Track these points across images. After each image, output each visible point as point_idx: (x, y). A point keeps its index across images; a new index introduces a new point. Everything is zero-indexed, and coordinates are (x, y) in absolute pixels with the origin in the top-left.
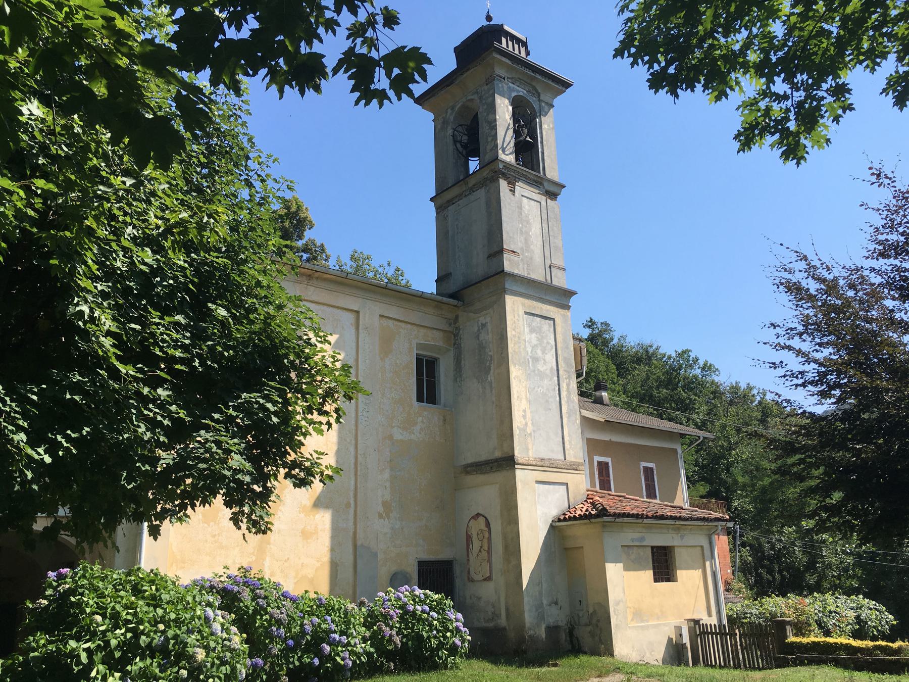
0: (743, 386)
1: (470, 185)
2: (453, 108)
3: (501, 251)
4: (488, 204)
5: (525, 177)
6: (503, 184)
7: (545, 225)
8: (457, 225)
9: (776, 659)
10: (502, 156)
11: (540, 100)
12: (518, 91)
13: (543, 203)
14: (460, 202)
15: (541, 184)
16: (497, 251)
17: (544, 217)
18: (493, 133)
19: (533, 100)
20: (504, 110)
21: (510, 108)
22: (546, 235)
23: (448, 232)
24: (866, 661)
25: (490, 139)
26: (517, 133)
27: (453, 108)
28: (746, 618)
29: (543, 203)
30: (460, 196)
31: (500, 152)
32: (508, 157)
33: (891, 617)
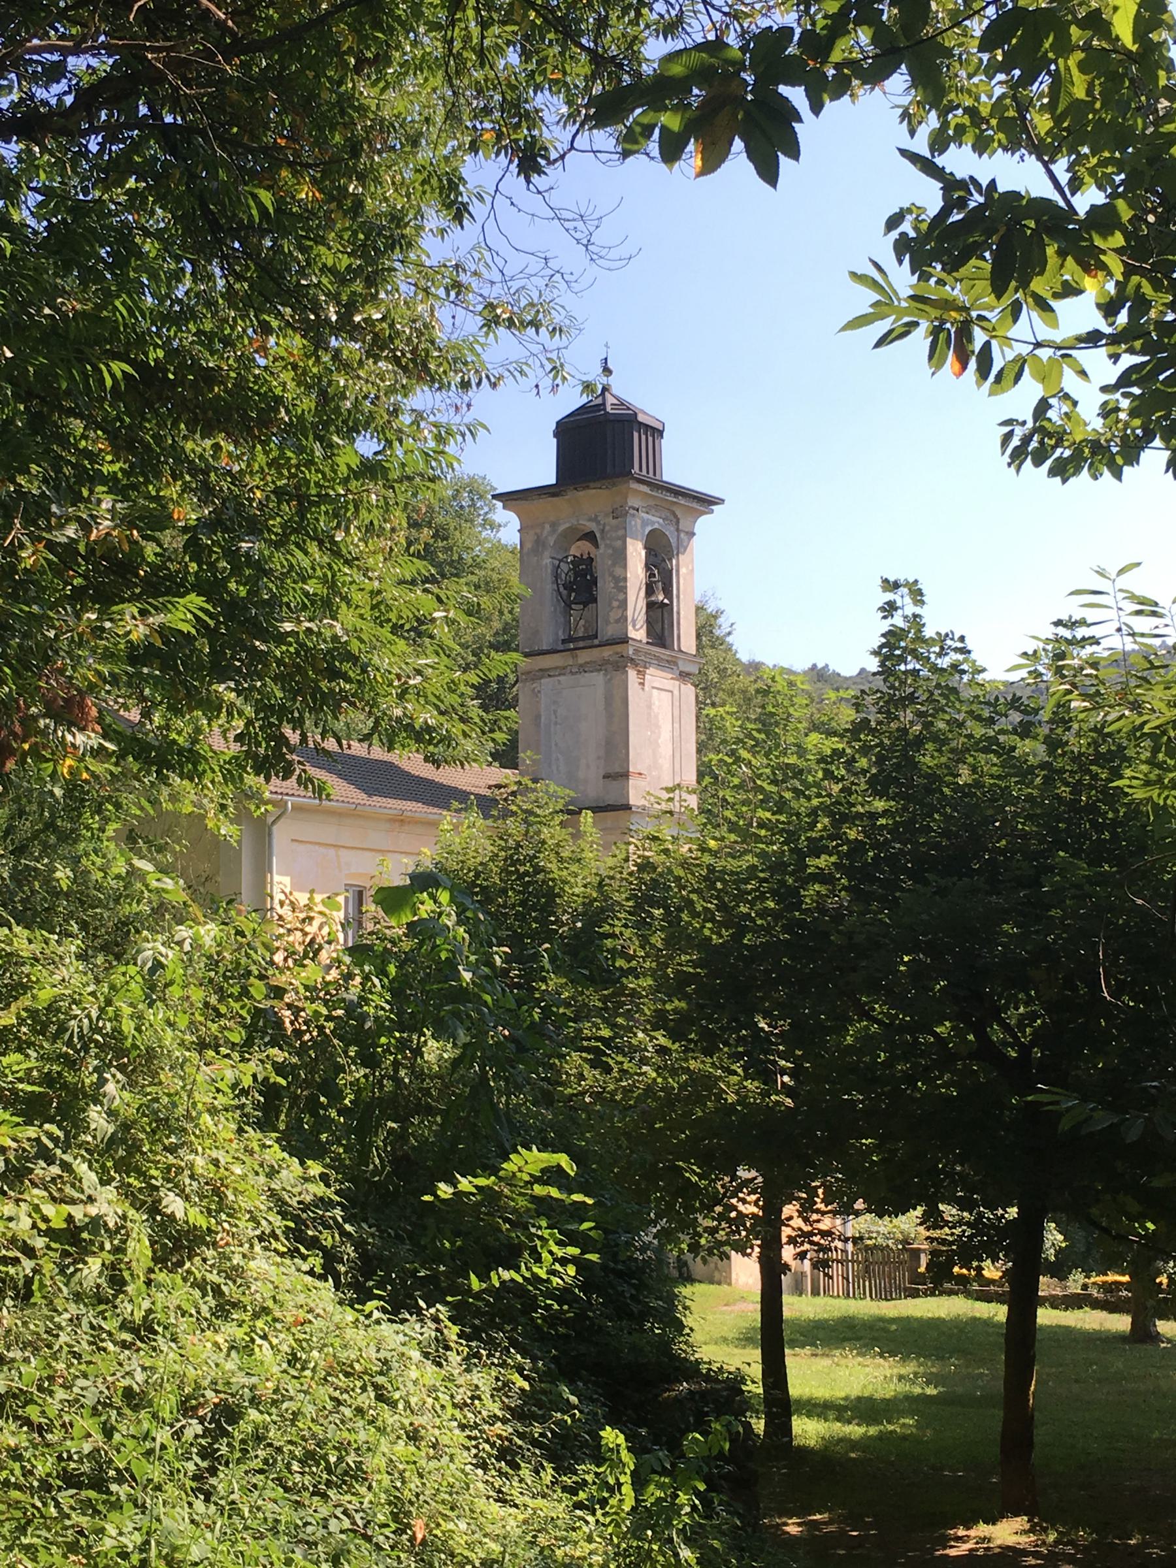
0: (820, 666)
1: (581, 661)
2: (554, 525)
3: (625, 775)
4: (608, 699)
5: (658, 658)
6: (632, 674)
7: (676, 725)
8: (555, 712)
9: (905, 1289)
10: (632, 634)
11: (678, 530)
12: (653, 523)
13: (676, 692)
14: (562, 678)
15: (676, 664)
16: (620, 776)
17: (676, 713)
18: (621, 597)
19: (670, 531)
20: (636, 553)
21: (643, 553)
22: (677, 739)
23: (538, 717)
24: (996, 1292)
25: (615, 604)
26: (650, 590)
27: (554, 525)
28: (870, 1238)
29: (676, 692)
30: (562, 670)
31: (630, 628)
32: (638, 633)
33: (1060, 1237)
